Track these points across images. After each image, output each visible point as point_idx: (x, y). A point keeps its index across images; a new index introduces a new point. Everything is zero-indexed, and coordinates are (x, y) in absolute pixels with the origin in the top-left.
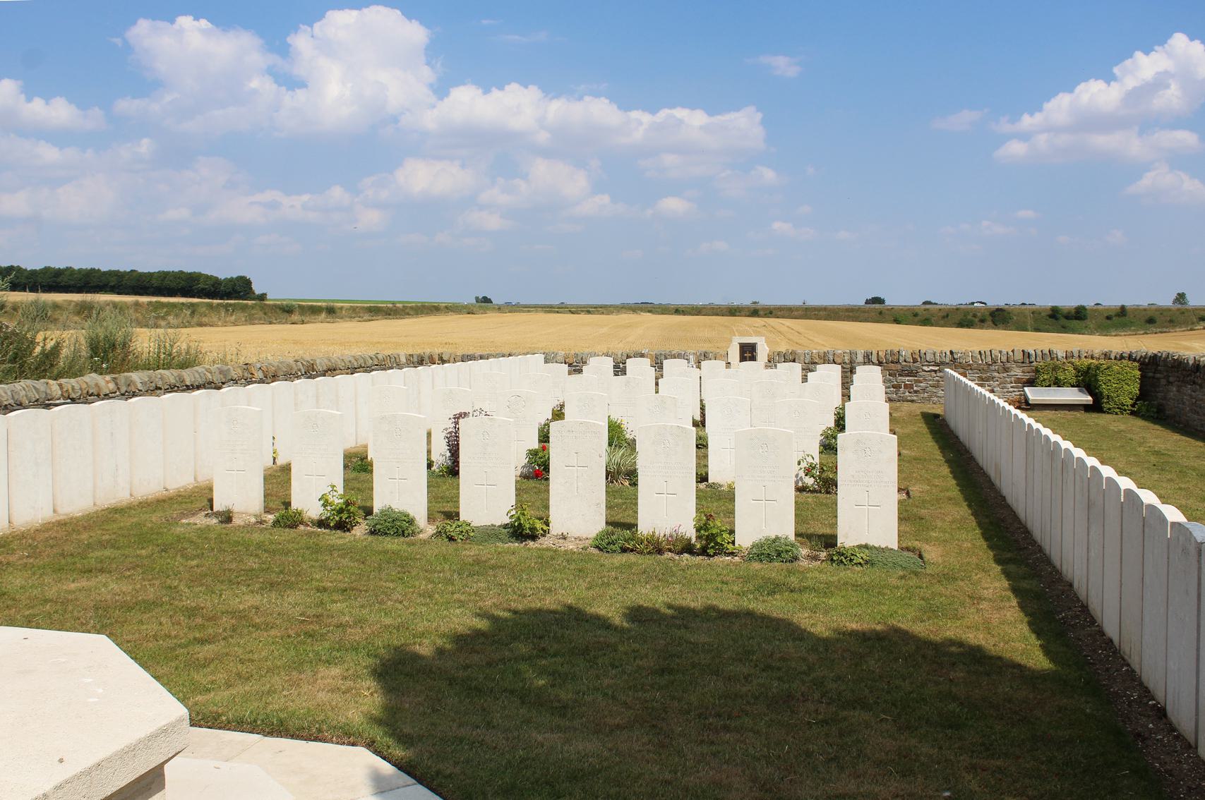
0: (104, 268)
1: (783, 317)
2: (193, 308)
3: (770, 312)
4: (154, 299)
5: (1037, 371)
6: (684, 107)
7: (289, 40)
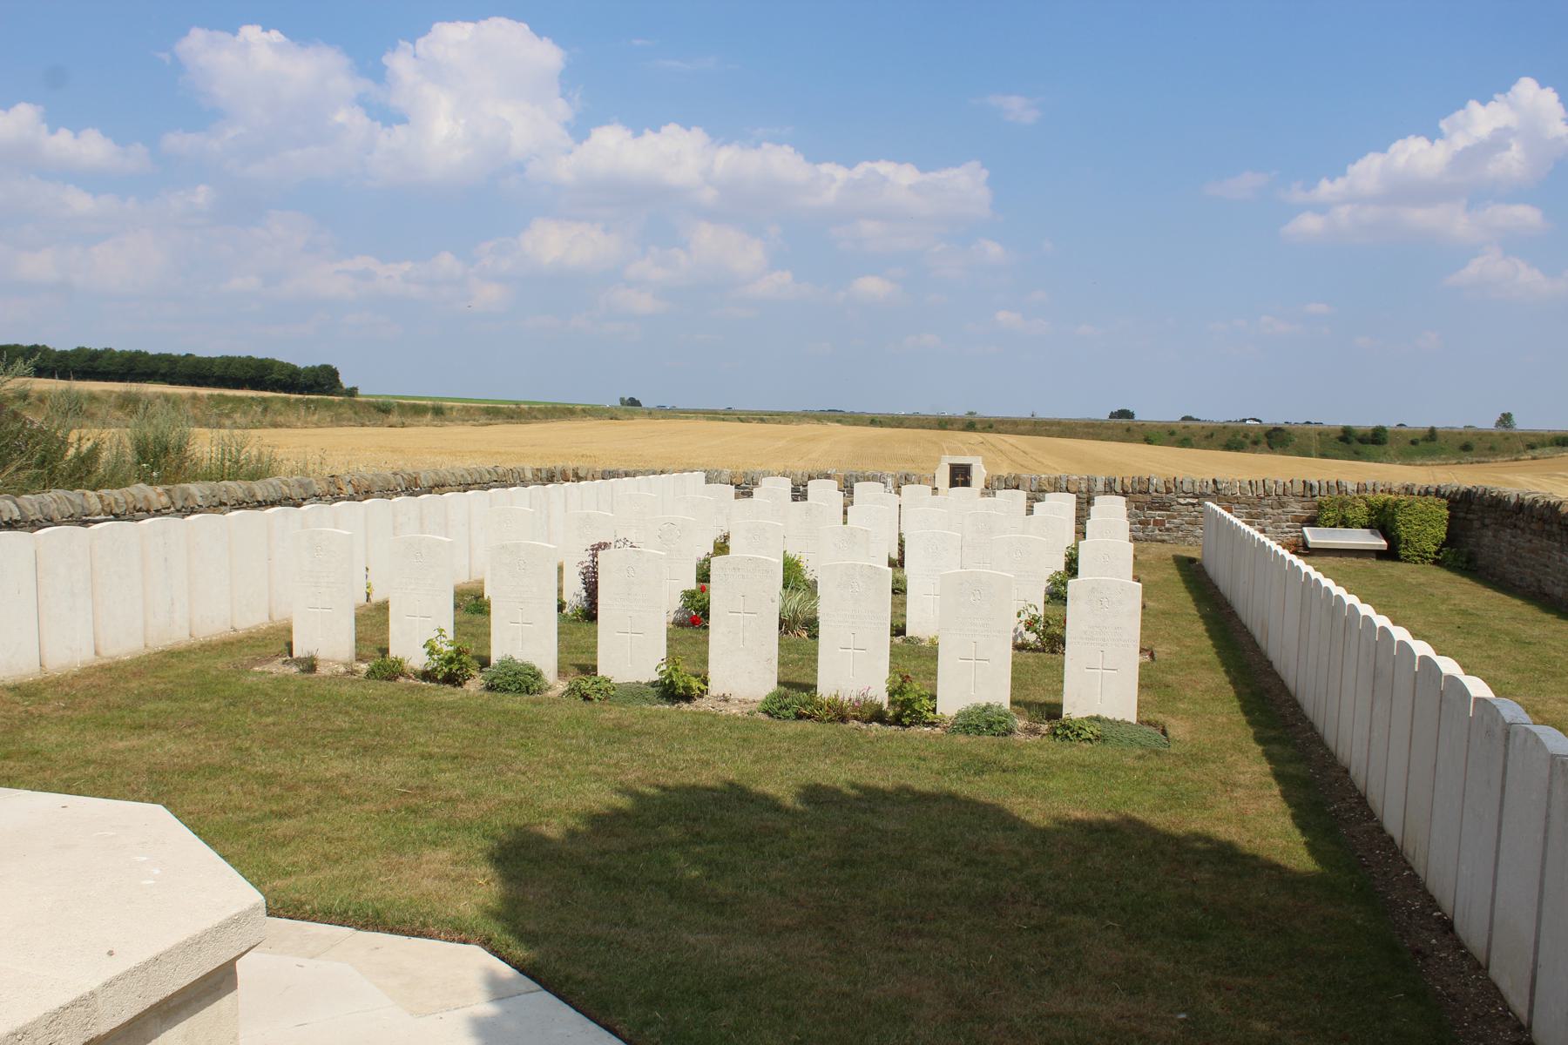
4: (216, 391)
5: (1320, 507)
6: (889, 160)
7: (385, 60)
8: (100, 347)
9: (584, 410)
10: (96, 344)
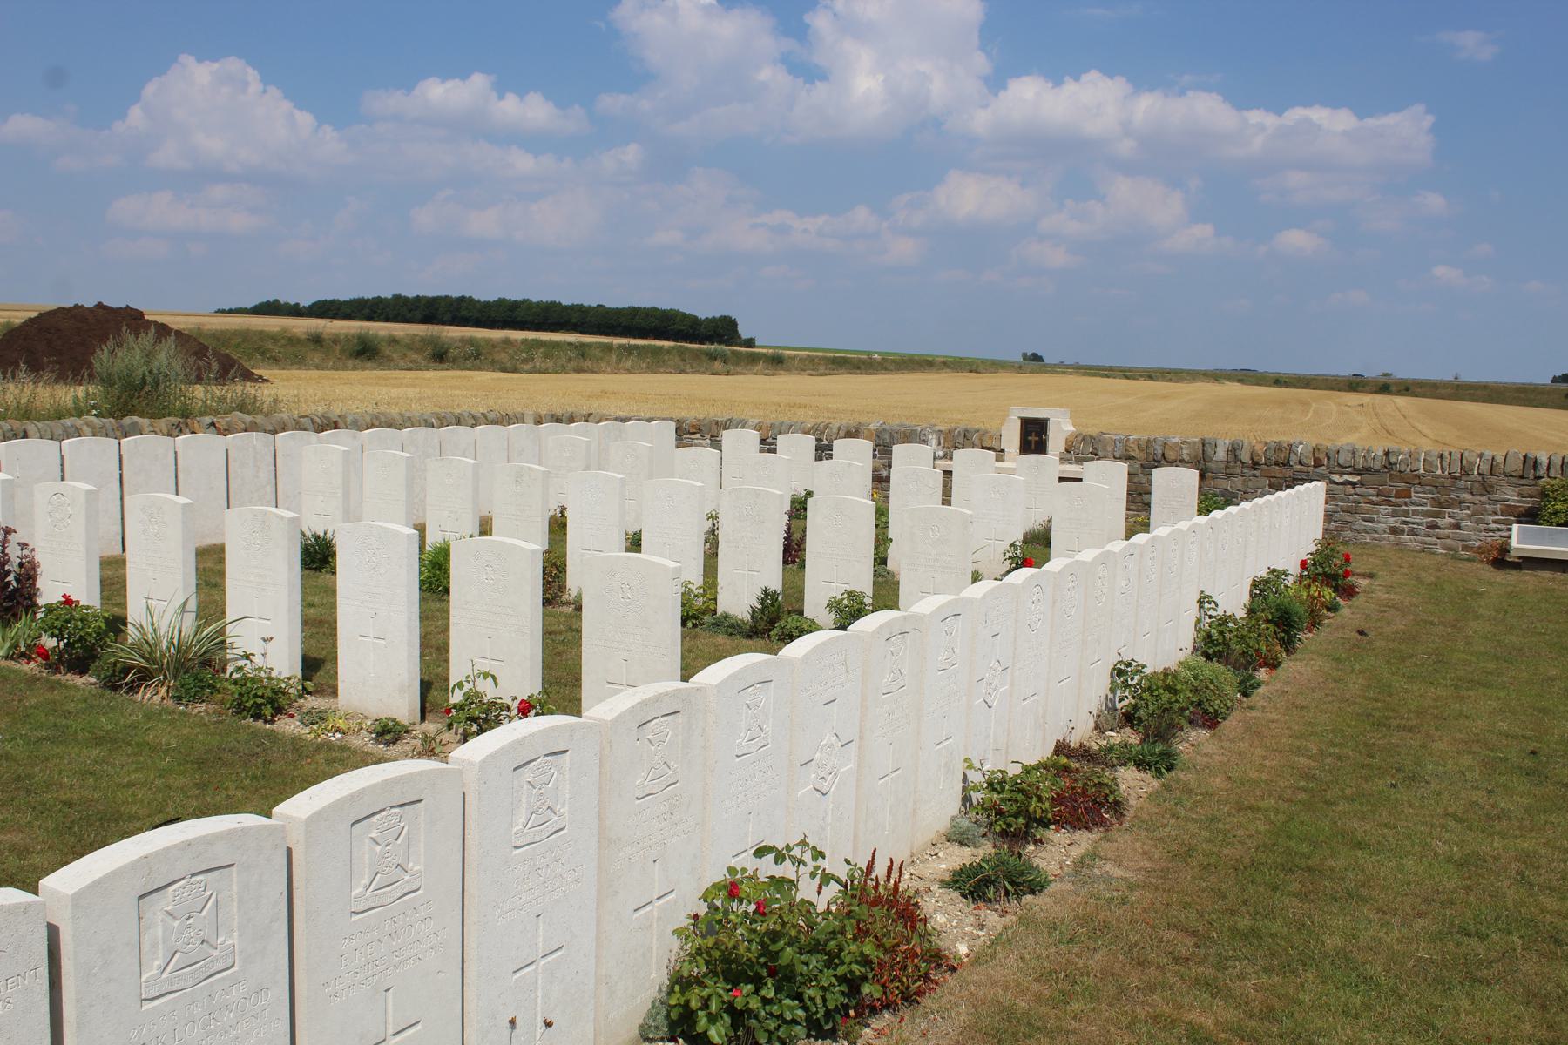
0: (566, 300)
1: (1424, 396)
2: (582, 350)
3: (1407, 389)
4: (623, 341)
5: (1544, 494)
7: (807, 18)
8: (520, 298)
9: (944, 363)
10: (515, 295)
